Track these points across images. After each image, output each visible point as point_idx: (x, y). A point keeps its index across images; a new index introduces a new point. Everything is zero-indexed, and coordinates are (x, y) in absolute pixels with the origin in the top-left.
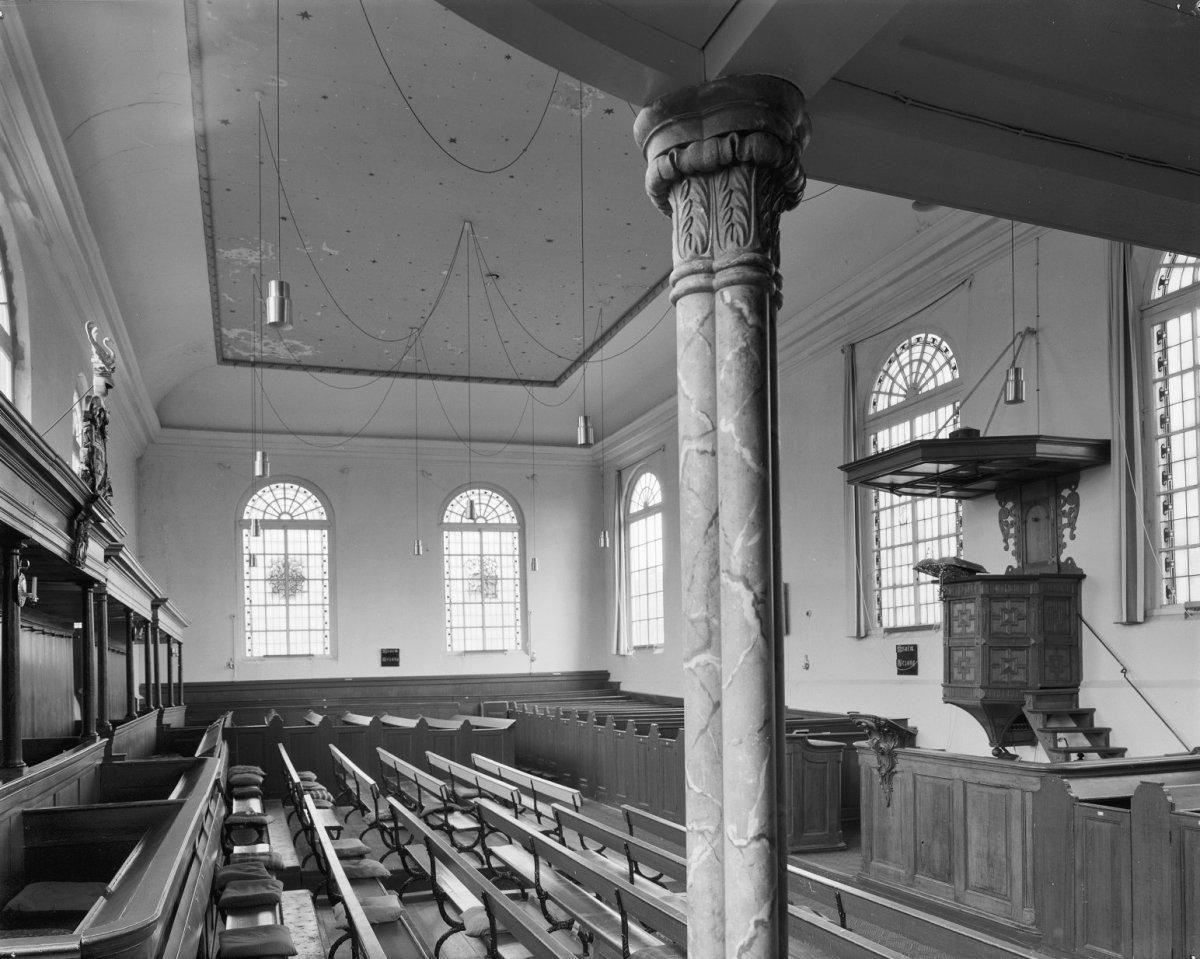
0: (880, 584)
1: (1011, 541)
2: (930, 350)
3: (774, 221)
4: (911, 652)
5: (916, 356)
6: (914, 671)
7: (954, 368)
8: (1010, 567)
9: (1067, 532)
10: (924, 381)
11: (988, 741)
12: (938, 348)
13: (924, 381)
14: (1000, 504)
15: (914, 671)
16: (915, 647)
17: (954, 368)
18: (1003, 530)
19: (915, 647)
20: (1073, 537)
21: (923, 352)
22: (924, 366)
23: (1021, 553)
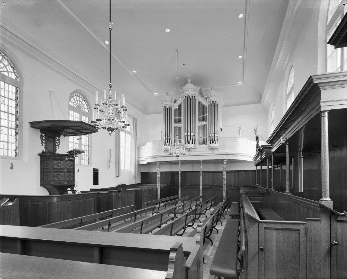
1: (44, 144)
3: (150, 232)
7: (81, 97)
9: (57, 147)
11: (75, 172)
14: (41, 133)
18: (41, 140)
20: (58, 149)
22: (76, 102)
23: (46, 148)
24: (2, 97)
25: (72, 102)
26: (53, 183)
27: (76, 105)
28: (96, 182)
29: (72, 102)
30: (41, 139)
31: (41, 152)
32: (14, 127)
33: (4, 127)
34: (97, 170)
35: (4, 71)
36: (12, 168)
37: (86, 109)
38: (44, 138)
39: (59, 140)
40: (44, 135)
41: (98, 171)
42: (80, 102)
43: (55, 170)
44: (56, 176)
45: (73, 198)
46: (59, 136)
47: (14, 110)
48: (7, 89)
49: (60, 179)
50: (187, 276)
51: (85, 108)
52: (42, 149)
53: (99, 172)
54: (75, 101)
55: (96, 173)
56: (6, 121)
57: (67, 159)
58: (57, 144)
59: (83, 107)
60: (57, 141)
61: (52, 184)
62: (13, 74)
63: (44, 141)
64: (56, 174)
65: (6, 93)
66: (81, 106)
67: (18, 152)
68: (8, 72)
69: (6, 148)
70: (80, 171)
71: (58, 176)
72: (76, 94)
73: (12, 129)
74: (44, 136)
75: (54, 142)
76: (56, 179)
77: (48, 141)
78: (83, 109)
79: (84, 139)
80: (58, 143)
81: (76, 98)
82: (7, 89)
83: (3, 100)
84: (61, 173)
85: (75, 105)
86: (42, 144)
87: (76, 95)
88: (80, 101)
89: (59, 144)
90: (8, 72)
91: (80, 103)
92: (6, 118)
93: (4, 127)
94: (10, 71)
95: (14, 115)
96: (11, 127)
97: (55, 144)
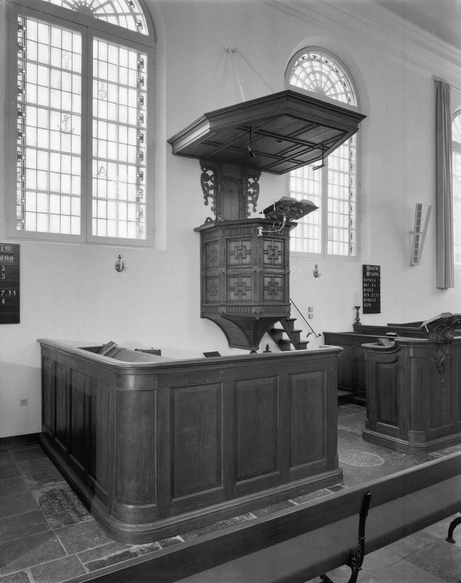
1: (211, 200)
5: (309, 70)
7: (327, 62)
9: (251, 206)
14: (202, 169)
18: (204, 189)
21: (304, 69)
23: (217, 210)
27: (311, 86)
28: (372, 305)
30: (204, 185)
31: (200, 223)
32: (133, 159)
33: (107, 161)
34: (376, 270)
35: (106, 15)
38: (210, 183)
39: (256, 186)
40: (210, 173)
41: (379, 272)
45: (222, 372)
46: (257, 176)
47: (133, 113)
48: (113, 59)
49: (244, 298)
51: (338, 92)
52: (203, 212)
53: (381, 276)
54: (308, 75)
55: (372, 281)
57: (260, 234)
58: (250, 198)
59: (332, 90)
61: (223, 313)
62: (130, 19)
63: (212, 192)
66: (326, 89)
68: (116, 15)
70: (319, 273)
72: (311, 55)
73: (128, 164)
74: (212, 176)
75: (240, 192)
77: (222, 190)
79: (336, 182)
80: (252, 195)
81: (312, 66)
83: (105, 89)
84: (244, 280)
86: (207, 200)
88: (321, 73)
89: (257, 198)
90: (116, 15)
91: (324, 79)
92: (112, 137)
93: (107, 161)
94: (122, 12)
95: (132, 126)
96: (125, 160)
97: (245, 198)
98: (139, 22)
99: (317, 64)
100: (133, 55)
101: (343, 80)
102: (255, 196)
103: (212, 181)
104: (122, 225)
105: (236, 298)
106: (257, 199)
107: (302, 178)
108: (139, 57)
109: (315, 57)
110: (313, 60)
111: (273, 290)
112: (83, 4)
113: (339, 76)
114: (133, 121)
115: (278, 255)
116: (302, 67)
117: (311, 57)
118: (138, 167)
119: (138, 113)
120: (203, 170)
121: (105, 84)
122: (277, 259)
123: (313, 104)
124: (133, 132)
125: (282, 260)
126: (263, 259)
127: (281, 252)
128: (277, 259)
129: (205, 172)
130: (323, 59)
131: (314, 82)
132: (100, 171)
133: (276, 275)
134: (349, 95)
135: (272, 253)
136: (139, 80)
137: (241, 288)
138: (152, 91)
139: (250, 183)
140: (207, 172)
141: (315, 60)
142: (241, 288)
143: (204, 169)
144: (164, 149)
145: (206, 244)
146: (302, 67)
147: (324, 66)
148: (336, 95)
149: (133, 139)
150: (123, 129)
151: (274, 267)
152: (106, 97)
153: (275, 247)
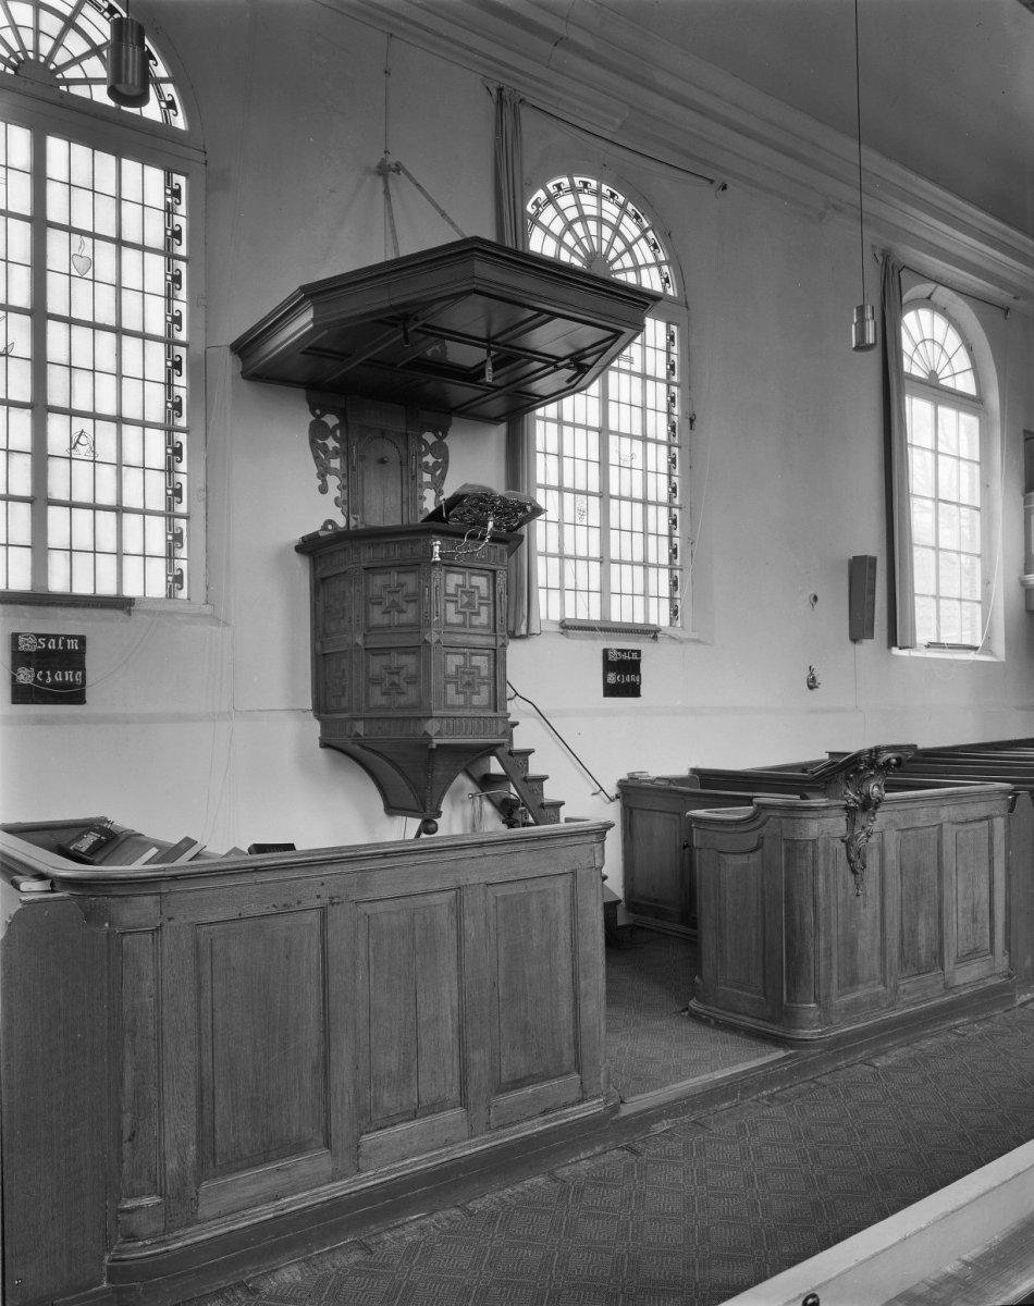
0: (671, 543)
1: (333, 482)
2: (566, 201)
4: (73, 652)
5: (572, 214)
6: (633, 690)
7: (613, 195)
8: (330, 522)
10: (605, 245)
12: (573, 190)
13: (605, 245)
15: (633, 690)
16: (82, 640)
17: (613, 195)
18: (316, 458)
19: (82, 640)
21: (560, 212)
23: (349, 504)
24: (75, 237)
25: (547, 231)
26: (360, 728)
27: (577, 249)
29: (547, 231)
30: (316, 447)
31: (313, 526)
32: (156, 413)
33: (94, 416)
36: (812, 684)
37: (647, 266)
38: (331, 443)
40: (331, 420)
42: (600, 230)
43: (374, 642)
44: (376, 681)
46: (442, 430)
47: (156, 307)
50: (128, 2)
54: (569, 226)
56: (107, 384)
60: (430, 459)
61: (358, 735)
64: (377, 665)
65: (106, 208)
66: (612, 255)
67: (183, 565)
69: (108, 542)
71: (387, 682)
74: (336, 427)
76: (378, 698)
78: (624, 270)
81: (578, 205)
82: (107, 184)
83: (88, 252)
85: (572, 252)
86: (324, 481)
87: (572, 184)
88: (600, 220)
89: (443, 477)
92: (107, 361)
93: (94, 416)
98: (170, 99)
99: (592, 200)
100: (155, 176)
101: (651, 234)
102: (438, 473)
103: (336, 439)
104: (132, 566)
105: (383, 702)
106: (444, 479)
107: (560, 421)
108: (168, 181)
109: (585, 184)
110: (580, 191)
111: (468, 684)
112: (31, 55)
113: (640, 226)
114: (157, 326)
115: (480, 604)
116: (557, 207)
117: (577, 185)
118: (169, 430)
119: (169, 308)
120: (314, 414)
121: (88, 241)
122: (478, 614)
123: (291, 868)
124: (157, 351)
125: (489, 617)
126: (445, 615)
127: (487, 598)
128: (478, 614)
129: (318, 417)
130: (605, 188)
131: (584, 241)
132: (78, 442)
133: (476, 650)
134: (665, 268)
135: (466, 599)
136: (169, 233)
137: (395, 679)
138: (201, 257)
139: (425, 443)
140: (323, 419)
141: (586, 191)
142: (395, 679)
143: (318, 412)
144: (227, 367)
145: (323, 579)
146: (557, 207)
147: (606, 204)
148: (637, 268)
149: (157, 369)
150: (131, 345)
151: (472, 631)
152: (91, 270)
153: (472, 587)
